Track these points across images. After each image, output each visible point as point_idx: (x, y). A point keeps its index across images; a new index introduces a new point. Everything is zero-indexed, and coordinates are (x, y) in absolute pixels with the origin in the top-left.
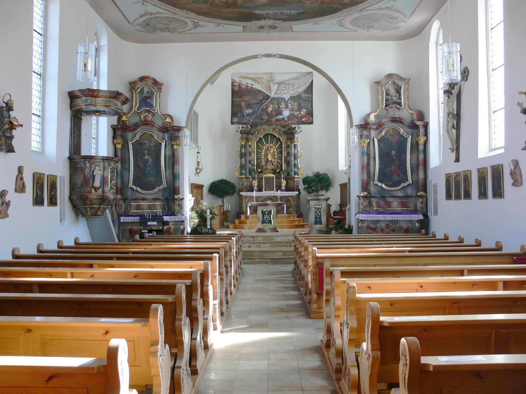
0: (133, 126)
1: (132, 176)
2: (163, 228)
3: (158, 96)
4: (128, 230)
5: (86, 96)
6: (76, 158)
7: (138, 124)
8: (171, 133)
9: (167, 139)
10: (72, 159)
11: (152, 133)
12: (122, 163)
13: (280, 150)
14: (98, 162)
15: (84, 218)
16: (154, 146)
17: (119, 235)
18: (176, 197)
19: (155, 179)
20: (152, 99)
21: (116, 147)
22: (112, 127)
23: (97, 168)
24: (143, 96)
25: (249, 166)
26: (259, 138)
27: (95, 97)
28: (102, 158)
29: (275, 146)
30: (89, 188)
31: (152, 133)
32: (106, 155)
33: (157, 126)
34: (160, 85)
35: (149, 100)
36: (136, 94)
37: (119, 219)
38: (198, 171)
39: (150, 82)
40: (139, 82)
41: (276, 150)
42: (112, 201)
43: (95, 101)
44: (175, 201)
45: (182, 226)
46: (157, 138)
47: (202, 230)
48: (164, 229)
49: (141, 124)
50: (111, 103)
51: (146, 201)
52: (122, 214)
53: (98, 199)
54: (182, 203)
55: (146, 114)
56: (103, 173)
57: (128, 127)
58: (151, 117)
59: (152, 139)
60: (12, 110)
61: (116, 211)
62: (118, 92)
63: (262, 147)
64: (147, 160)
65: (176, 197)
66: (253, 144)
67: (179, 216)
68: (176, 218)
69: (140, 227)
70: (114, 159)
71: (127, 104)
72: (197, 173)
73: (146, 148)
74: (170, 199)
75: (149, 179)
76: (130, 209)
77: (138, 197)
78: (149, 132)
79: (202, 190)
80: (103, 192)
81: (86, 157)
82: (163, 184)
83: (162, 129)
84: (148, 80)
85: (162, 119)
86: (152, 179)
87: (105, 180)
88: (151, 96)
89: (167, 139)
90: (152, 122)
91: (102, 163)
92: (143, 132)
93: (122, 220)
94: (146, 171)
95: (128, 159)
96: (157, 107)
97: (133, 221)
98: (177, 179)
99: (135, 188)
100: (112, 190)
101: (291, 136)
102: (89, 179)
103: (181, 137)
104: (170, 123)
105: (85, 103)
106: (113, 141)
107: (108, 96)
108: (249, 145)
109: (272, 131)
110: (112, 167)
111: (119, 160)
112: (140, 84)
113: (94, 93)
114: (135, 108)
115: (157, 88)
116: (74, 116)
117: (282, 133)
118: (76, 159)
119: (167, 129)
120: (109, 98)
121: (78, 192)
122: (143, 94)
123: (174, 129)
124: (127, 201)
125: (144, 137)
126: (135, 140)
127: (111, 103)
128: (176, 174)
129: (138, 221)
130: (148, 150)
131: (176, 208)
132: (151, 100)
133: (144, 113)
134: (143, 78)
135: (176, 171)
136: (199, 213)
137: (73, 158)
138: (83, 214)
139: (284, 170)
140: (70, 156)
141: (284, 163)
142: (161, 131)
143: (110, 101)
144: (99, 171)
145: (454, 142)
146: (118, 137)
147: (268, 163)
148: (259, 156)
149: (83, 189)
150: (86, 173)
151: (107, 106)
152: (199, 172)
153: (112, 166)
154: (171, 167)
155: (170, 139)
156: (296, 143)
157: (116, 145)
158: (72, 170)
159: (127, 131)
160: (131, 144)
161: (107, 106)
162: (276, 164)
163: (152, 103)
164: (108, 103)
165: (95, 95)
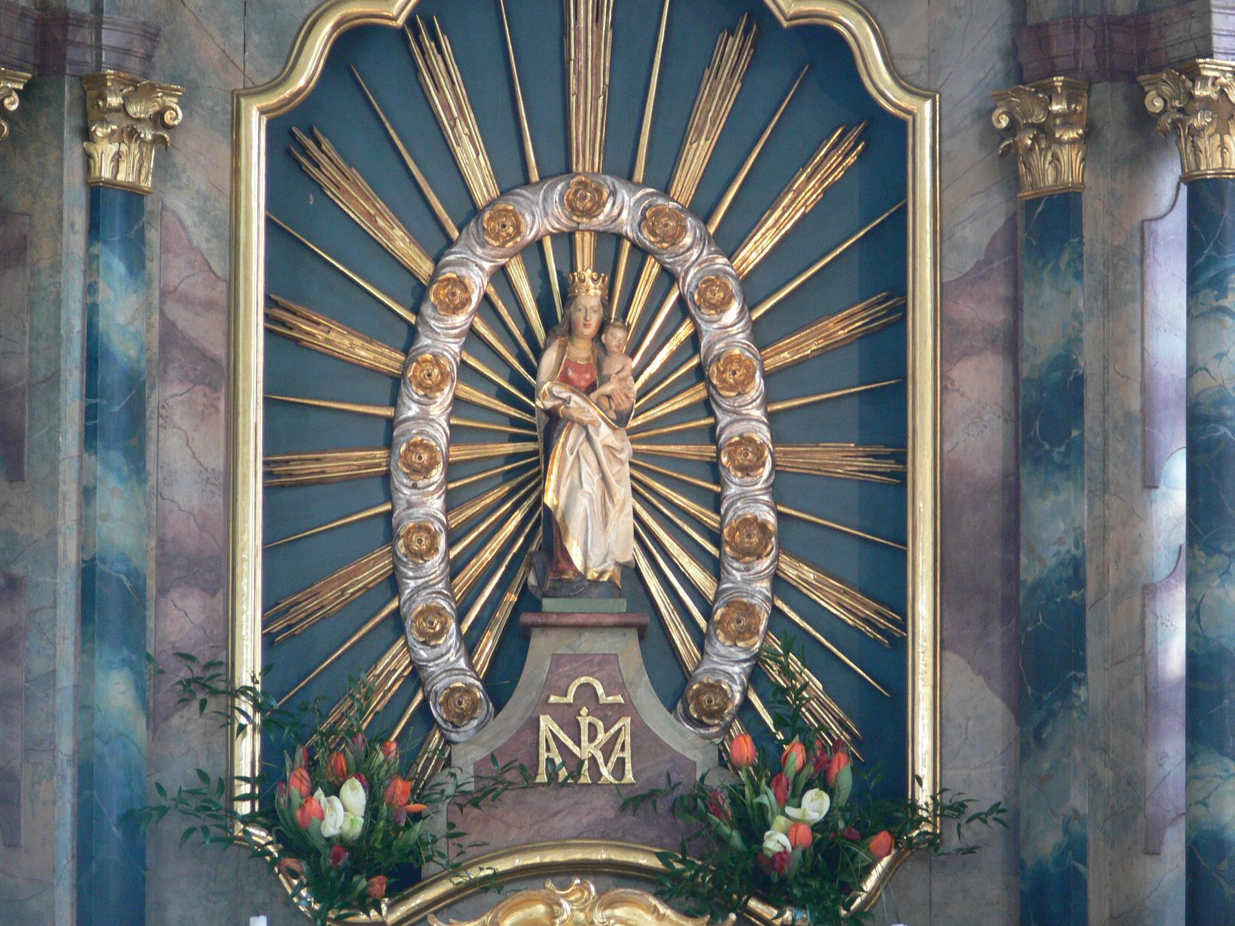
13: (330, 595)
25: (85, 706)
29: (729, 241)
41: (762, 334)
63: (400, 243)
108: (97, 193)
111: (499, 224)
139: (949, 809)
141: (942, 645)
145: (558, 178)
147: (541, 646)
148: (338, 464)
162: (756, 676)
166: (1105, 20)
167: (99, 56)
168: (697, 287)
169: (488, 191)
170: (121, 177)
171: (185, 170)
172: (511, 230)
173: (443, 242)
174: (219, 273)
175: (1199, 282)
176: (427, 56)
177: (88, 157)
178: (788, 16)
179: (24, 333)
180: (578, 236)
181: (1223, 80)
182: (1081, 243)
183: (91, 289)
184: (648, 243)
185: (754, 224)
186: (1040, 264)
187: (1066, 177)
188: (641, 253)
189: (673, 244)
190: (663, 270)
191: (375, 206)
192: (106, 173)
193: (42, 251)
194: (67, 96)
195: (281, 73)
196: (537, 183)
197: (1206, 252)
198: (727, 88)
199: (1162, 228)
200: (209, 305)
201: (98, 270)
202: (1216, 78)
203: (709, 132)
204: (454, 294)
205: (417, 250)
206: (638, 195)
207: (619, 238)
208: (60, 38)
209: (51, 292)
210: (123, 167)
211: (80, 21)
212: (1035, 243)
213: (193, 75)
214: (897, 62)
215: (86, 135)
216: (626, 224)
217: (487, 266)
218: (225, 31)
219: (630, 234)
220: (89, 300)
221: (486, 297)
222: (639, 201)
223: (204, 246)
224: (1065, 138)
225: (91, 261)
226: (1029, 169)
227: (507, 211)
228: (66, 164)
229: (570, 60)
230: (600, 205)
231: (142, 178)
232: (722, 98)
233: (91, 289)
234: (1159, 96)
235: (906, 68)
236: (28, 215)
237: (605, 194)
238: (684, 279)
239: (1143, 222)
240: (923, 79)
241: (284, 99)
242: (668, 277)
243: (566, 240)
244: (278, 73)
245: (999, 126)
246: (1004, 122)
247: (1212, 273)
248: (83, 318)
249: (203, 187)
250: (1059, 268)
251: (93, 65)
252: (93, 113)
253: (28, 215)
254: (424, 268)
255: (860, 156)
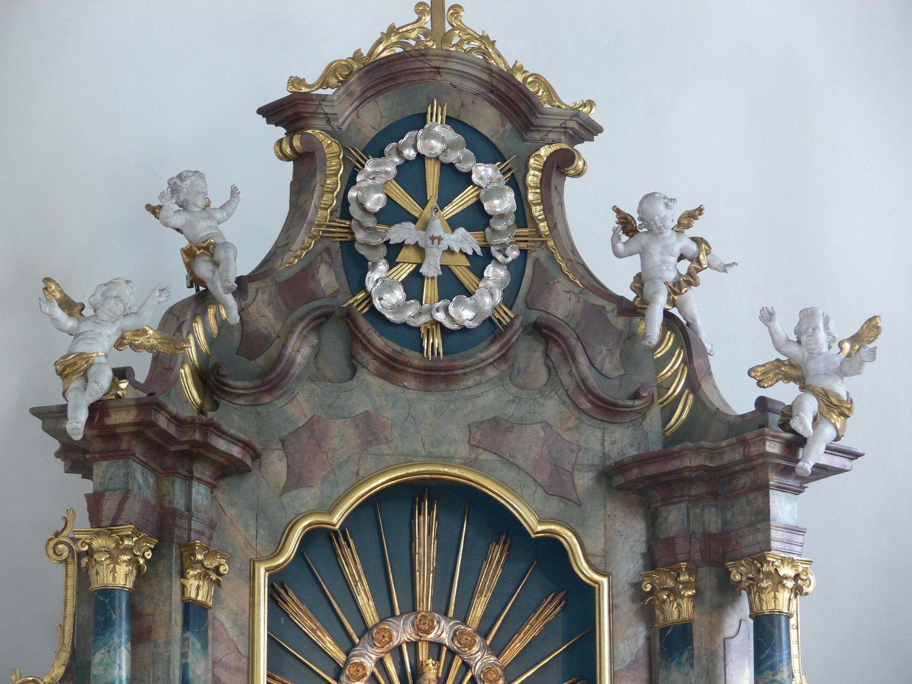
26: (309, 537)
60: (358, 52)
66: (234, 589)
101: (712, 520)
109: (463, 451)
117: (584, 480)
156: (782, 601)
166: (707, 535)
167: (189, 535)
168: (482, 671)
169: (374, 619)
170: (199, 598)
171: (225, 599)
172: (387, 639)
173: (350, 645)
174: (243, 654)
175: (762, 668)
176: (342, 549)
177: (183, 587)
178: (535, 531)
179: (150, 677)
180: (420, 644)
181: (777, 563)
182: (693, 649)
183: (184, 655)
184: (455, 647)
185: (510, 640)
186: (670, 660)
187: (685, 615)
188: (452, 653)
189: (470, 649)
190: (464, 663)
191: (315, 624)
192: (193, 596)
193: (160, 634)
194: (174, 554)
195: (276, 551)
196: (399, 616)
197: (767, 651)
198: (495, 570)
199: (734, 644)
200: (238, 669)
201: (188, 646)
202: (773, 562)
203: (487, 593)
204: (358, 671)
205: (337, 648)
206: (451, 624)
207: (440, 645)
208: (171, 523)
209: (165, 656)
210: (200, 593)
211: (181, 515)
212: (666, 649)
213: (230, 550)
214: (589, 557)
215: (183, 575)
216: (446, 638)
217: (374, 657)
218: (247, 528)
219: (447, 644)
220: (183, 661)
221: (373, 674)
222: (451, 626)
223: (235, 639)
224: (686, 595)
225: (184, 640)
226: (663, 612)
227: (385, 629)
228: (173, 589)
229: (416, 554)
230: (433, 628)
231: (208, 600)
232: (493, 577)
233: (184, 655)
234: (738, 573)
235: (596, 561)
236: (152, 615)
237: (435, 623)
238: (475, 667)
239: (725, 639)
240: (602, 567)
241: (272, 567)
242: (466, 666)
243: (414, 646)
244: (275, 550)
245: (644, 589)
246: (649, 588)
247: (769, 663)
248: (180, 671)
249: (235, 608)
250: (681, 662)
251: (186, 539)
252: (187, 564)
253: (152, 615)
254: (341, 657)
255: (562, 608)
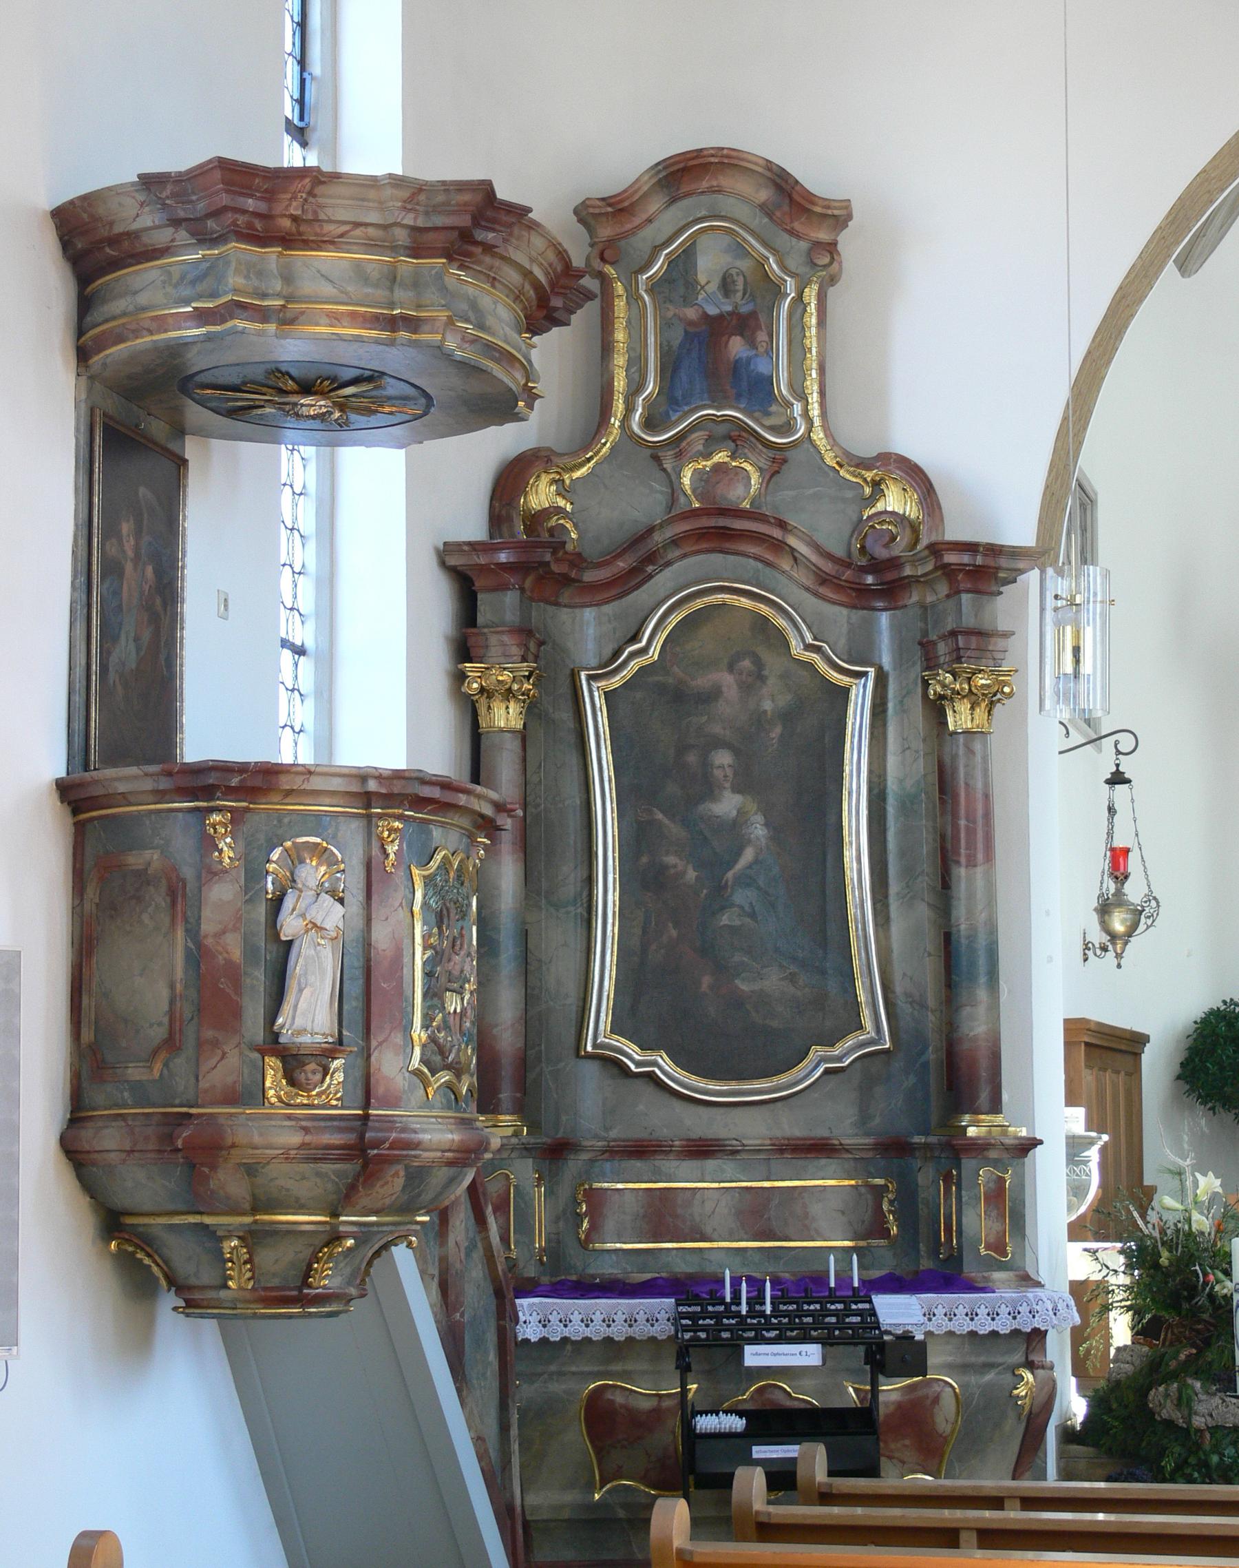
0: (619, 556)
1: (611, 959)
2: (875, 1391)
3: (812, 308)
4: (578, 1409)
5: (206, 239)
6: (122, 787)
7: (658, 538)
8: (924, 607)
9: (886, 661)
10: (93, 802)
11: (764, 609)
12: (526, 848)
14: (316, 823)
15: (209, 1328)
16: (788, 717)
17: (506, 1464)
18: (972, 1132)
19: (792, 978)
20: (762, 336)
21: (483, 723)
22: (443, 564)
23: (312, 873)
24: (691, 313)
27: (287, 241)
28: (355, 788)
30: (233, 1059)
31: (764, 609)
32: (402, 765)
33: (803, 548)
34: (824, 216)
35: (737, 347)
36: (633, 297)
37: (506, 1316)
38: (1119, 927)
39: (745, 200)
40: (654, 205)
42: (443, 1174)
43: (288, 278)
44: (968, 1164)
45: (1028, 1376)
46: (808, 647)
47: (1191, 1412)
48: (882, 1398)
49: (675, 542)
50: (431, 296)
51: (728, 1166)
52: (531, 1272)
53: (315, 1155)
54: (1020, 1186)
55: (721, 457)
56: (359, 923)
57: (578, 560)
58: (755, 479)
59: (773, 664)
61: (478, 1254)
62: (486, 190)
64: (735, 829)
65: (972, 1132)
67: (1006, 1294)
68: (982, 1311)
69: (683, 1386)
70: (462, 799)
71: (566, 323)
72: (1113, 937)
73: (717, 729)
74: (927, 1146)
75: (744, 987)
76: (593, 1227)
77: (664, 1133)
78: (745, 602)
79: (1135, 1072)
80: (366, 1088)
81: (212, 780)
82: (860, 1027)
83: (848, 574)
84: (725, 181)
85: (849, 494)
86: (772, 982)
87: (381, 984)
88: (753, 315)
89: (886, 661)
90: (762, 518)
91: (352, 832)
92: (699, 604)
93: (530, 1330)
94: (725, 920)
95: (574, 822)
96: (804, 398)
97: (619, 1332)
98: (973, 978)
99: (632, 1054)
100: (445, 1077)
102: (234, 974)
103: (1007, 635)
104: (914, 527)
105: (199, 297)
106: (460, 678)
107: (402, 236)
110: (445, 865)
111: (499, 807)
112: (668, 219)
113: (278, 209)
114: (630, 409)
115: (804, 245)
116: (107, 429)
118: (125, 799)
119: (890, 576)
120: (416, 251)
121: (141, 1094)
122: (687, 300)
123: (949, 572)
124: (574, 1165)
125: (703, 642)
126: (634, 665)
127: (431, 296)
128: (972, 938)
129: (663, 1329)
130: (736, 752)
131: (969, 1219)
132: (752, 344)
133: (700, 447)
134: (685, 170)
135: (970, 913)
136: (1156, 1266)
137: (98, 791)
138: (190, 1288)
140: (80, 775)
142: (839, 588)
143: (416, 284)
144: (327, 900)
146: (493, 640)
149: (180, 1063)
150: (208, 927)
151: (392, 323)
152: (1130, 933)
153: (438, 857)
154: (926, 881)
155: (918, 652)
157: (482, 710)
158: (91, 892)
159: (566, 596)
160: (600, 701)
161: (392, 323)
163: (762, 367)
164: (399, 294)
165: (286, 223)
